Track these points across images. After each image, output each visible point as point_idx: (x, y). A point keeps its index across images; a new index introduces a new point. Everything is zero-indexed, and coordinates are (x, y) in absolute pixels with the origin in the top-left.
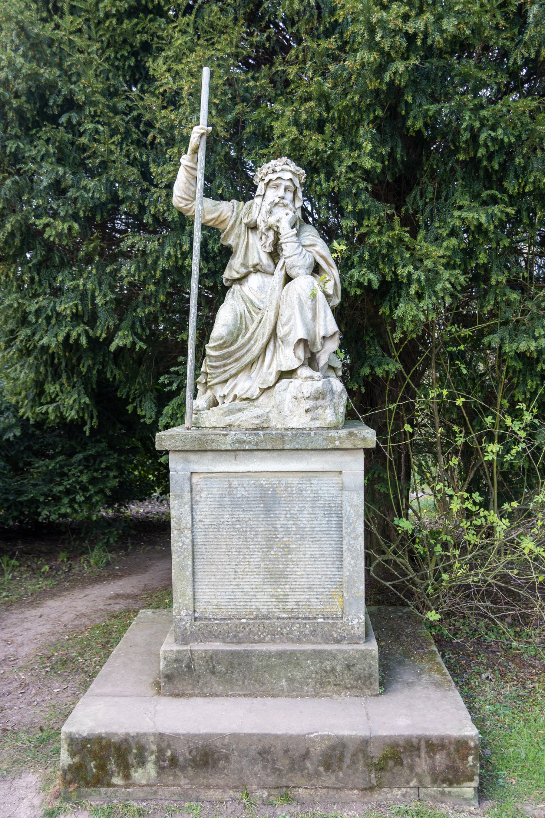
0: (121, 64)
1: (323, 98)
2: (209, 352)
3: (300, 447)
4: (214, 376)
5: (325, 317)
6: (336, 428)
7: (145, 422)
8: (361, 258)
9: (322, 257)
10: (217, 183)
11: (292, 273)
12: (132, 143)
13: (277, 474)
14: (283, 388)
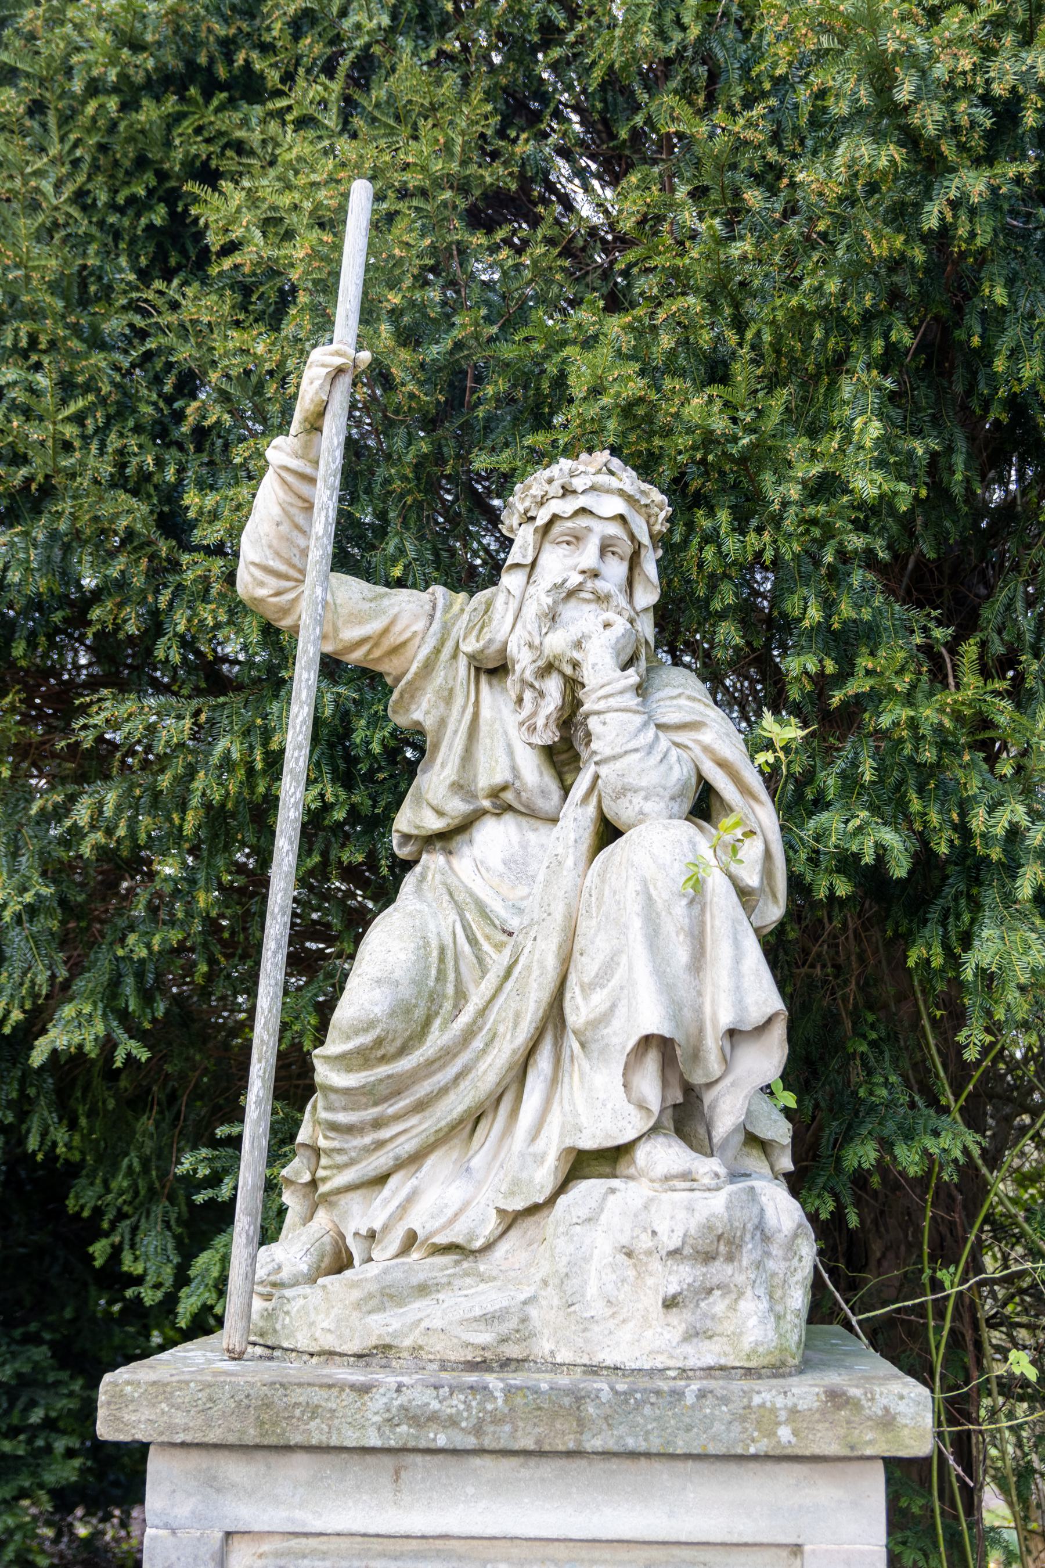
0: (126, 223)
1: (727, 293)
2: (324, 1073)
3: (642, 1446)
4: (340, 1159)
5: (737, 960)
6: (777, 1370)
7: (138, 1299)
8: (850, 781)
9: (723, 764)
10: (391, 549)
11: (620, 812)
12: (138, 429)
13: (551, 1550)
14: (583, 1212)
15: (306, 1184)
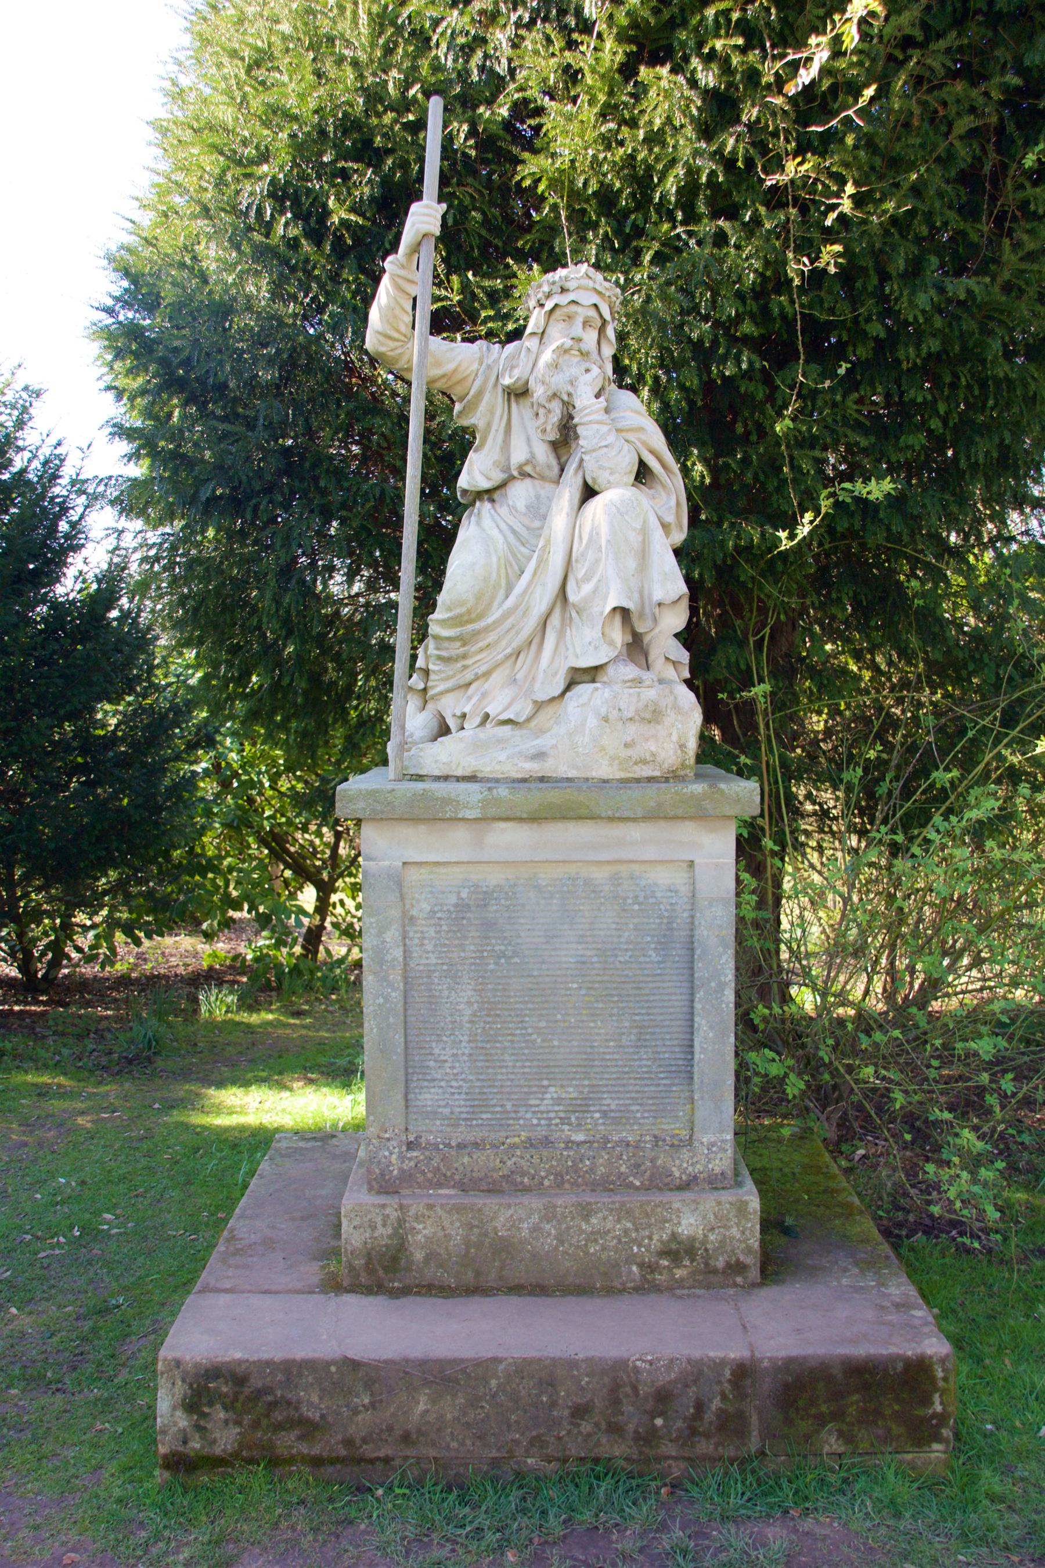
2: (434, 629)
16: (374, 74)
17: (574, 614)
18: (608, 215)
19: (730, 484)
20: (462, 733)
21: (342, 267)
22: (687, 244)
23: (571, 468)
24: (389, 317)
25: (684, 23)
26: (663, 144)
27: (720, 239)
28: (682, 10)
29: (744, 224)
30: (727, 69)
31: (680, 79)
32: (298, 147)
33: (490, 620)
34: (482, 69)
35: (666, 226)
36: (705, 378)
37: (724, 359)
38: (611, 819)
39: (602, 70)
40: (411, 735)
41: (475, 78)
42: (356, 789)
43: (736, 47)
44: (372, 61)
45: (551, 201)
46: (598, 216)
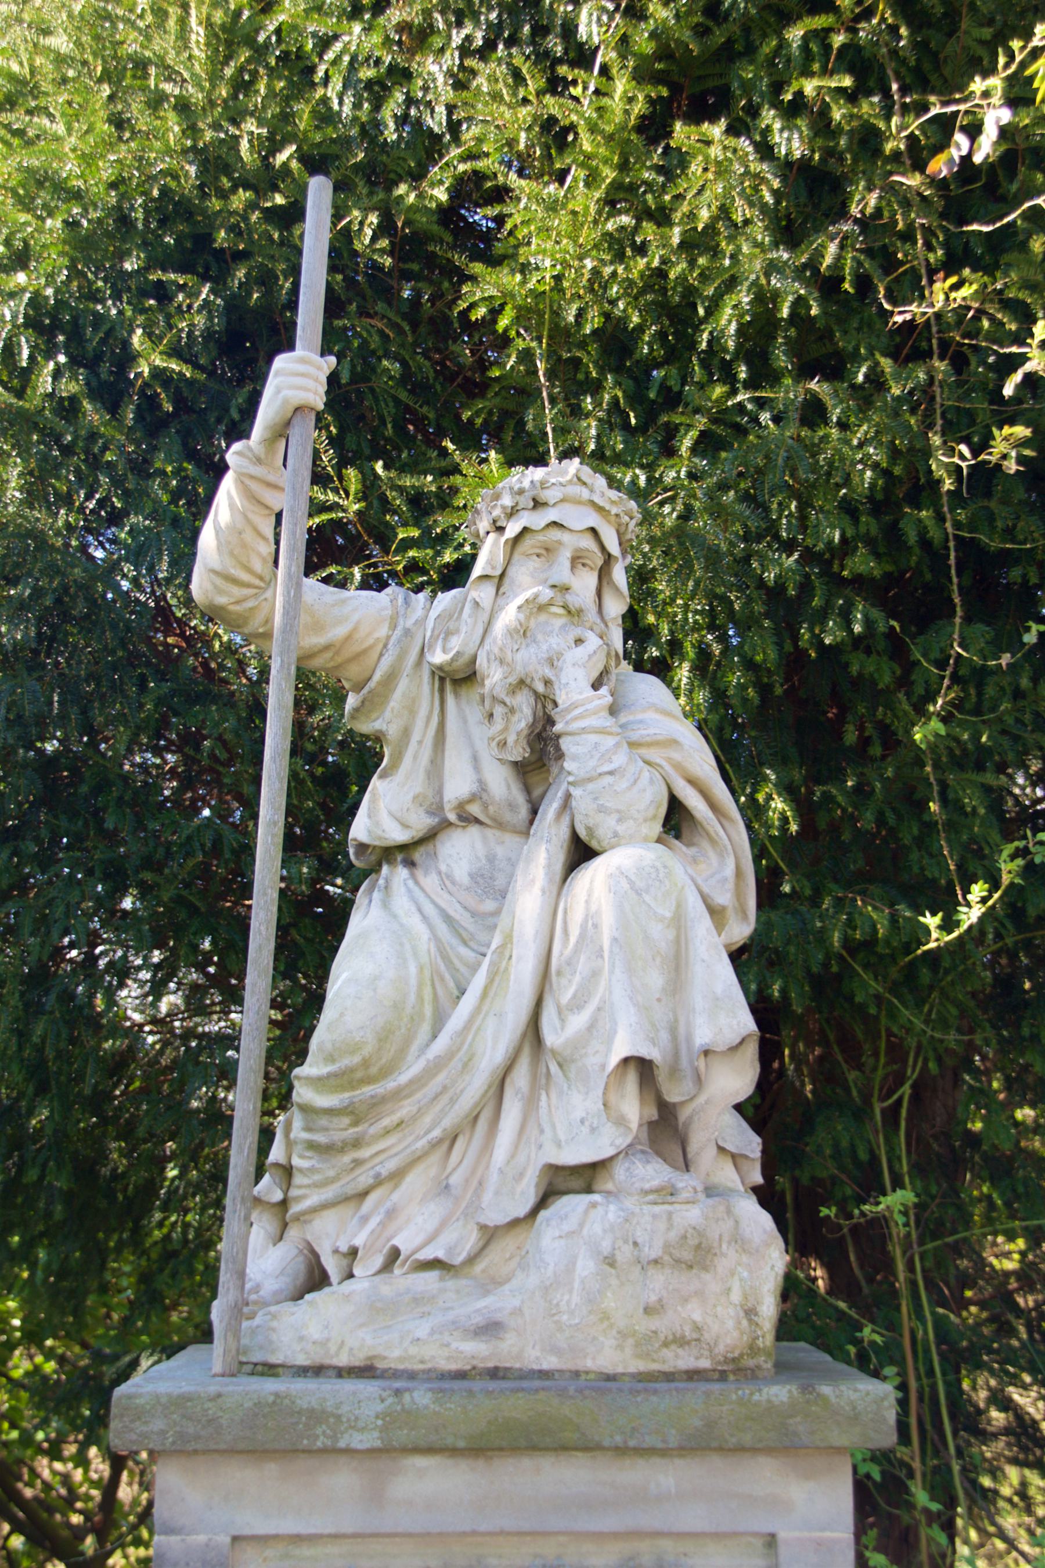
2: (302, 1093)
15: (275, 1205)
16: (216, 126)
17: (554, 1068)
18: (618, 370)
19: (835, 828)
20: (349, 1286)
21: (154, 449)
22: (755, 420)
23: (550, 809)
24: (229, 543)
25: (750, 51)
26: (716, 253)
27: (814, 412)
28: (747, 30)
29: (853, 386)
30: (822, 126)
31: (744, 144)
32: (81, 244)
33: (403, 1078)
34: (402, 120)
35: (718, 391)
36: (788, 647)
37: (822, 616)
38: (621, 1451)
39: (609, 129)
40: (257, 1289)
41: (391, 135)
42: (153, 1383)
43: (840, 91)
44: (212, 103)
45: (521, 344)
46: (602, 371)
